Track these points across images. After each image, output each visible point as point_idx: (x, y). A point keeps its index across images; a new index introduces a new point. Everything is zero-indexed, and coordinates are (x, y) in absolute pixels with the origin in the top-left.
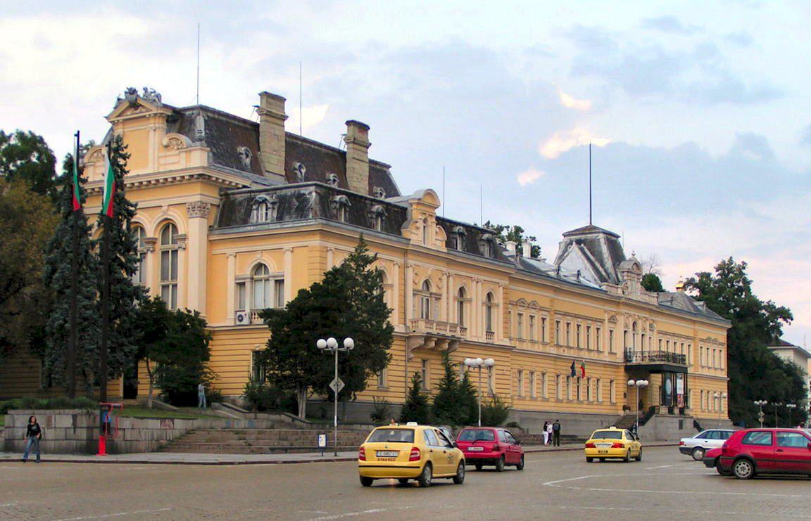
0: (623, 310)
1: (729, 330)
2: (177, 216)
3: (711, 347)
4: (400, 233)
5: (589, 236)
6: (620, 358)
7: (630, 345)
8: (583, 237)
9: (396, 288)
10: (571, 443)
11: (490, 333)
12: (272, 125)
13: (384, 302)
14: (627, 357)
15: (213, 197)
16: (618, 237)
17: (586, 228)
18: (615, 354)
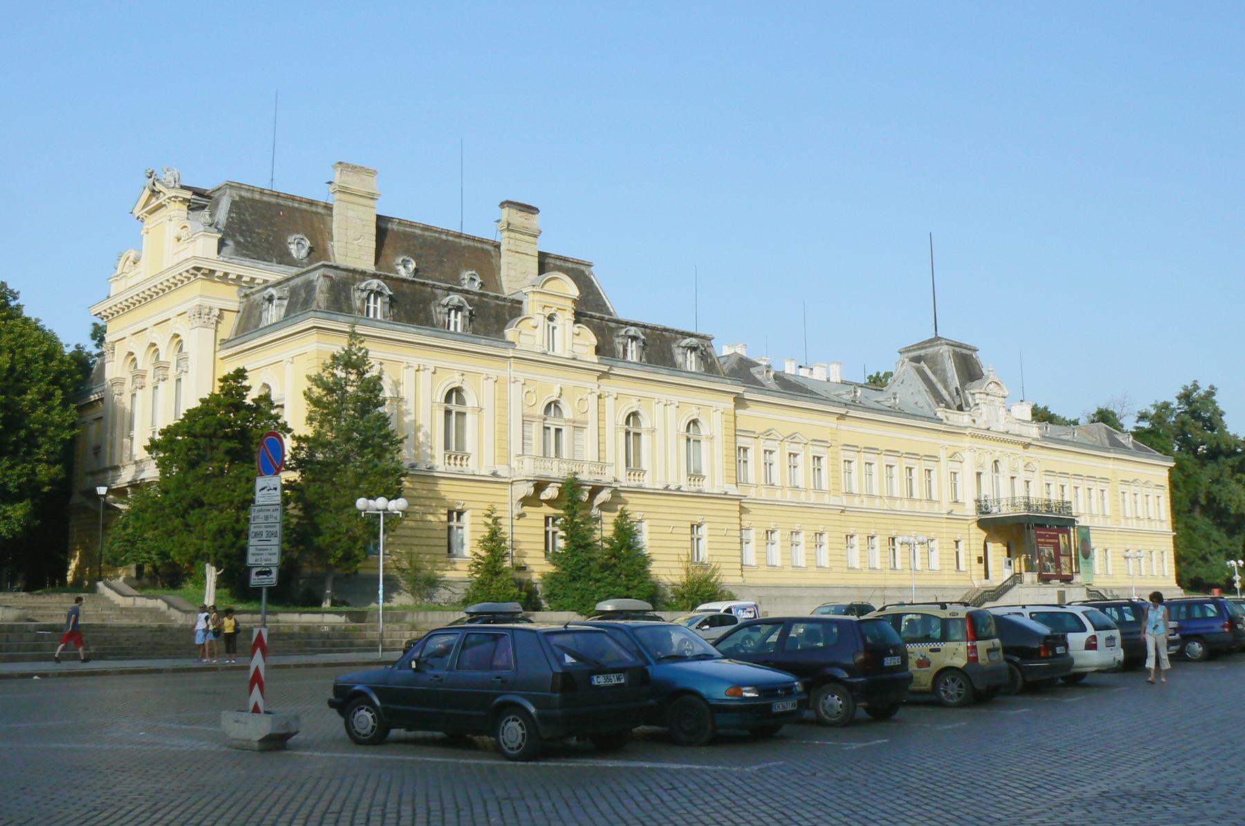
0: (966, 442)
1: (1171, 470)
2: (181, 326)
3: (1142, 491)
4: (503, 337)
5: (930, 350)
6: (970, 510)
7: (986, 490)
8: (922, 352)
9: (487, 415)
10: (348, 651)
11: (696, 475)
12: (350, 206)
13: (199, 404)
14: (981, 507)
15: (229, 298)
16: (975, 350)
17: (930, 341)
18: (964, 504)
